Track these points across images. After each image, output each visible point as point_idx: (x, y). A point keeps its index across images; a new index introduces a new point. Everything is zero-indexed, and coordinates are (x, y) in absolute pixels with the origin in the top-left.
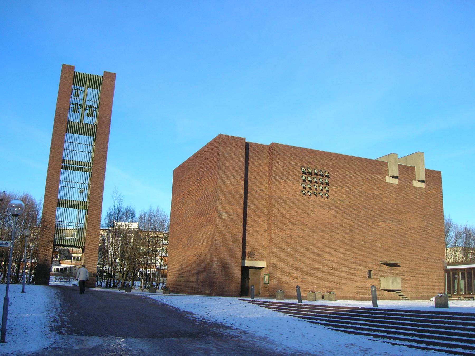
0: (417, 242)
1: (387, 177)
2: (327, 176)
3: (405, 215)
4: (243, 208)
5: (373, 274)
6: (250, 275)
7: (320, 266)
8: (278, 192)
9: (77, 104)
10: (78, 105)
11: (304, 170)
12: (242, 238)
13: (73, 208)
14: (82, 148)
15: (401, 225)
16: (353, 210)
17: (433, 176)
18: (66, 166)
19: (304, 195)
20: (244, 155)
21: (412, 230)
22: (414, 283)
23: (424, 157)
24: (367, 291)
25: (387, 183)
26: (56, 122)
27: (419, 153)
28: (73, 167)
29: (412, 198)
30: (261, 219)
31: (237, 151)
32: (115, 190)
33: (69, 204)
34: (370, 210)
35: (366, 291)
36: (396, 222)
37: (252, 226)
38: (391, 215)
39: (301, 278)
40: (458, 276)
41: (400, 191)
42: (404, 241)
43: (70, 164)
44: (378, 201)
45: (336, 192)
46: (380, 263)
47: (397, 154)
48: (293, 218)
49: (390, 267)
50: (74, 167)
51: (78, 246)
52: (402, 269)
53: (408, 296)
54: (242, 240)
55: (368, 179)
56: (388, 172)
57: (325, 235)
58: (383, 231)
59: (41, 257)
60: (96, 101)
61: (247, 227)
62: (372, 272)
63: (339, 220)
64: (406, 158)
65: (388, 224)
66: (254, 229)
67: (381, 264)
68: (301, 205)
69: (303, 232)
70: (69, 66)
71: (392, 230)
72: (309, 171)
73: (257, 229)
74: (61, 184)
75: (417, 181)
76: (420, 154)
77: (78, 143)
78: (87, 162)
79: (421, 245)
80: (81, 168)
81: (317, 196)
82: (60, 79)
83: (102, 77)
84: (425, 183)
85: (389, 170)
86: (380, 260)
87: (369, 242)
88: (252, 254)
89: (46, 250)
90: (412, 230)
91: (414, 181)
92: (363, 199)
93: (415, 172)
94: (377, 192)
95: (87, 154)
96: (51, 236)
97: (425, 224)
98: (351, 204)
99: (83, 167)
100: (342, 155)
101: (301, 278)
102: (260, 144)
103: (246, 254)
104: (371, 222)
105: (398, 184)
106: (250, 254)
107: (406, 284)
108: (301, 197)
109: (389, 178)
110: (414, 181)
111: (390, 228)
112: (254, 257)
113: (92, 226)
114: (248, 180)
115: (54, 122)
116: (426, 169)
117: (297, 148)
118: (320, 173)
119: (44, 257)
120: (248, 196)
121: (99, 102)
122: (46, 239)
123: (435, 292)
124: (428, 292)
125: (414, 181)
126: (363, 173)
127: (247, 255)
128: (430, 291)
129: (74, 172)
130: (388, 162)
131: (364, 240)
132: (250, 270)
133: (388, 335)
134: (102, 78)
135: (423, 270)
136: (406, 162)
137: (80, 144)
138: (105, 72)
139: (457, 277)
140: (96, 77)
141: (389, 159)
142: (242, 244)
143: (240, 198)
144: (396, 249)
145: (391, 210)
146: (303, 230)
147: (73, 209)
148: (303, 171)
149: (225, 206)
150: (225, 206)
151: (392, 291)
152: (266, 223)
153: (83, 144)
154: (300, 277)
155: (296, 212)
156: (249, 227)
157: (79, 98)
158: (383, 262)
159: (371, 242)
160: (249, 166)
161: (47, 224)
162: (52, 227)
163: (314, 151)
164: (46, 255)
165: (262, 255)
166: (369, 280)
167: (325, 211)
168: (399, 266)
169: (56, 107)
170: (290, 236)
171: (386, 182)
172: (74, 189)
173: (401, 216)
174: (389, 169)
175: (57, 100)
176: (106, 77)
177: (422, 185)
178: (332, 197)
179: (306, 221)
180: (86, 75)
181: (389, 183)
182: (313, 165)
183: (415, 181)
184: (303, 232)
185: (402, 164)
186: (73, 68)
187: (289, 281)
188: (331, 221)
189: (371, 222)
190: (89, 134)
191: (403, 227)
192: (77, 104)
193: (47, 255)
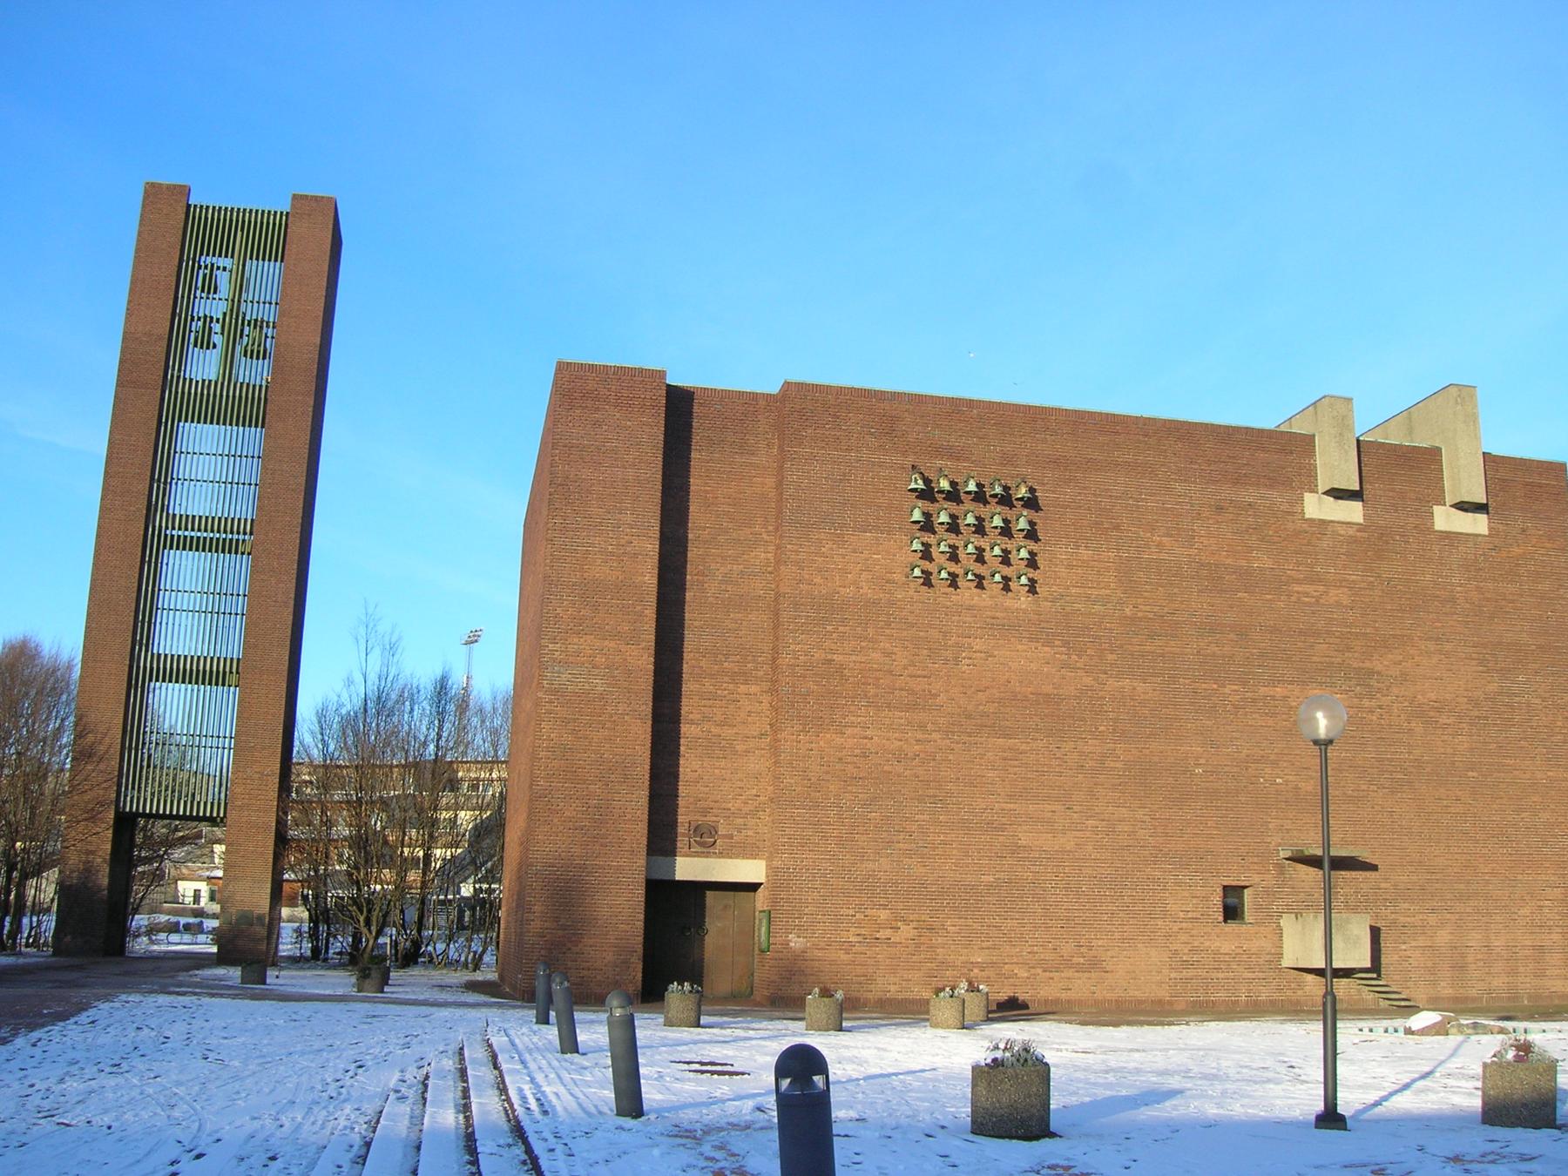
1: (1308, 496)
2: (1032, 503)
3: (1397, 651)
6: (707, 914)
9: (208, 319)
10: (211, 321)
11: (916, 480)
12: (647, 767)
13: (177, 682)
15: (1378, 695)
18: (231, 540)
19: (923, 584)
20: (662, 437)
21: (1432, 714)
22: (1443, 937)
23: (1475, 406)
24: (1221, 975)
26: (121, 384)
27: (1454, 390)
30: (743, 688)
31: (630, 421)
33: (205, 671)
34: (1232, 636)
35: (1214, 975)
36: (1353, 682)
38: (1332, 654)
39: (914, 924)
41: (1369, 553)
43: (173, 528)
44: (1269, 597)
45: (1070, 566)
46: (1282, 854)
47: (1350, 400)
48: (878, 679)
51: (222, 819)
52: (1386, 880)
53: (1419, 995)
54: (647, 776)
55: (1220, 509)
56: (1316, 473)
59: (74, 859)
60: (256, 299)
61: (682, 721)
62: (1246, 896)
63: (1088, 680)
64: (1410, 419)
66: (715, 730)
67: (1287, 859)
69: (920, 736)
70: (169, 187)
72: (941, 485)
74: (240, 604)
75: (1451, 506)
76: (1461, 395)
78: (226, 519)
79: (1475, 774)
80: (205, 538)
81: (984, 588)
82: (136, 233)
84: (1488, 513)
85: (1318, 466)
86: (1280, 845)
87: (1226, 769)
88: (705, 830)
89: (91, 836)
91: (1437, 510)
92: (1200, 591)
93: (1442, 470)
94: (1262, 561)
95: (232, 487)
96: (104, 785)
97: (1493, 687)
98: (1140, 614)
99: (212, 535)
100: (1100, 414)
101: (914, 924)
102: (740, 394)
103: (681, 830)
104: (1236, 687)
105: (1362, 521)
106: (695, 831)
110: (1437, 510)
112: (715, 842)
115: (117, 386)
116: (1494, 453)
118: (992, 493)
119: (84, 858)
120: (687, 598)
122: (87, 797)
123: (1548, 973)
124: (1513, 972)
125: (1435, 507)
126: (1195, 482)
127: (684, 835)
130: (1314, 436)
131: (1202, 761)
134: (284, 218)
135: (1488, 882)
138: (295, 197)
142: (647, 793)
144: (1355, 794)
145: (1328, 632)
148: (913, 486)
149: (576, 640)
150: (576, 640)
152: (766, 705)
153: (214, 455)
156: (692, 722)
157: (216, 296)
158: (1289, 854)
161: (93, 743)
162: (112, 751)
163: (971, 403)
164: (89, 853)
165: (750, 833)
166: (1232, 926)
167: (1020, 647)
168: (1374, 868)
169: (125, 333)
171: (1307, 516)
173: (1376, 656)
174: (1318, 462)
175: (128, 309)
176: (297, 213)
177: (1478, 524)
178: (1055, 588)
179: (933, 691)
180: (247, 215)
181: (1320, 520)
182: (967, 459)
184: (920, 736)
185: (1379, 440)
186: (185, 191)
188: (1048, 689)
189: (1236, 687)
190: (241, 419)
191: (1385, 701)
192: (208, 319)
193: (92, 852)
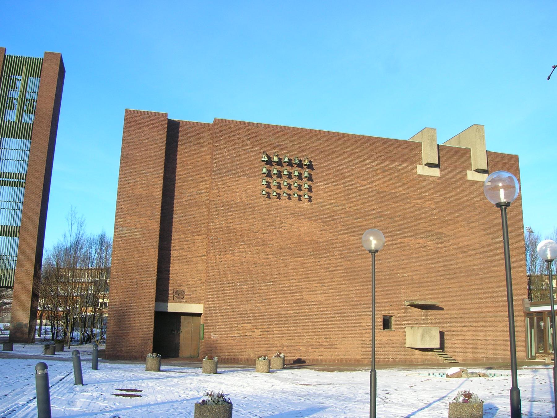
0: (475, 269)
1: (418, 166)
4: (159, 221)
5: (394, 323)
7: (296, 311)
8: (221, 194)
11: (264, 157)
14: (13, 155)
15: (445, 243)
16: (356, 219)
17: (503, 163)
22: (469, 336)
24: (382, 350)
25: (419, 175)
28: (4, 181)
29: (465, 198)
32: (72, 211)
34: (388, 219)
36: (435, 237)
37: (181, 249)
39: (261, 330)
40: (545, 323)
41: (442, 188)
42: (449, 268)
45: (325, 191)
47: (435, 129)
49: (424, 310)
50: (5, 181)
52: (447, 314)
54: (156, 271)
55: (384, 170)
57: (305, 261)
58: (412, 253)
61: (172, 250)
65: (421, 241)
67: (408, 305)
68: (262, 213)
71: (428, 250)
72: (274, 159)
73: (189, 254)
76: (479, 128)
77: (10, 149)
79: (482, 273)
83: (42, 59)
85: (423, 154)
86: (405, 300)
87: (385, 270)
90: (465, 250)
92: (376, 202)
94: (400, 190)
98: (352, 210)
99: (15, 180)
103: (170, 292)
104: (389, 239)
105: (439, 176)
107: (454, 338)
108: (262, 201)
109: (423, 167)
111: (424, 247)
112: (184, 297)
113: (24, 259)
114: (177, 178)
116: (491, 151)
117: (258, 125)
121: (36, 92)
125: (468, 171)
127: (171, 294)
128: (499, 348)
129: (4, 187)
130: (421, 143)
132: (182, 317)
133: (541, 405)
135: (486, 315)
136: (459, 142)
137: (12, 149)
138: (46, 53)
139: (542, 325)
140: (34, 60)
141: (422, 137)
143: (154, 205)
144: (435, 280)
145: (425, 218)
146: (265, 253)
147: (3, 237)
149: (129, 218)
150: (129, 218)
151: (429, 350)
154: (258, 329)
155: (252, 224)
156: (175, 250)
159: (388, 271)
160: (178, 156)
165: (198, 293)
166: (386, 331)
168: (442, 309)
170: (242, 264)
171: (418, 174)
172: (3, 210)
174: (422, 153)
179: (270, 239)
181: (423, 175)
183: (471, 171)
184: (264, 256)
187: (239, 335)
188: (315, 239)
191: (447, 245)
